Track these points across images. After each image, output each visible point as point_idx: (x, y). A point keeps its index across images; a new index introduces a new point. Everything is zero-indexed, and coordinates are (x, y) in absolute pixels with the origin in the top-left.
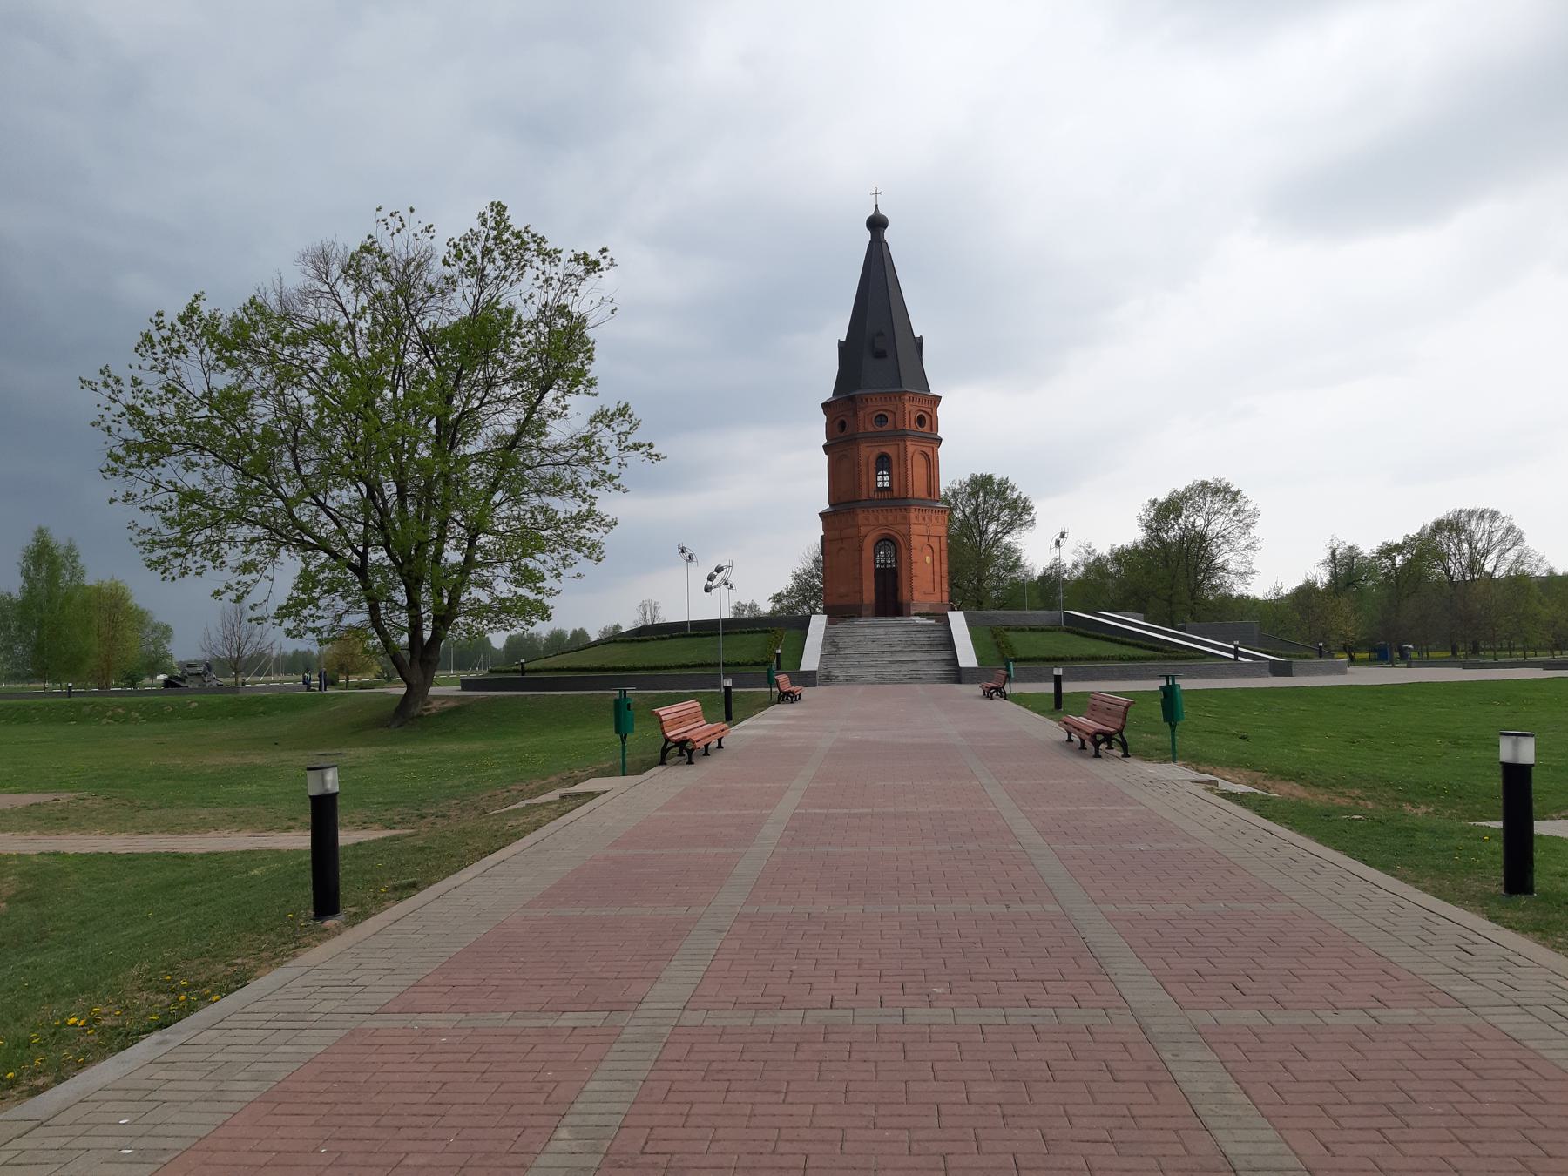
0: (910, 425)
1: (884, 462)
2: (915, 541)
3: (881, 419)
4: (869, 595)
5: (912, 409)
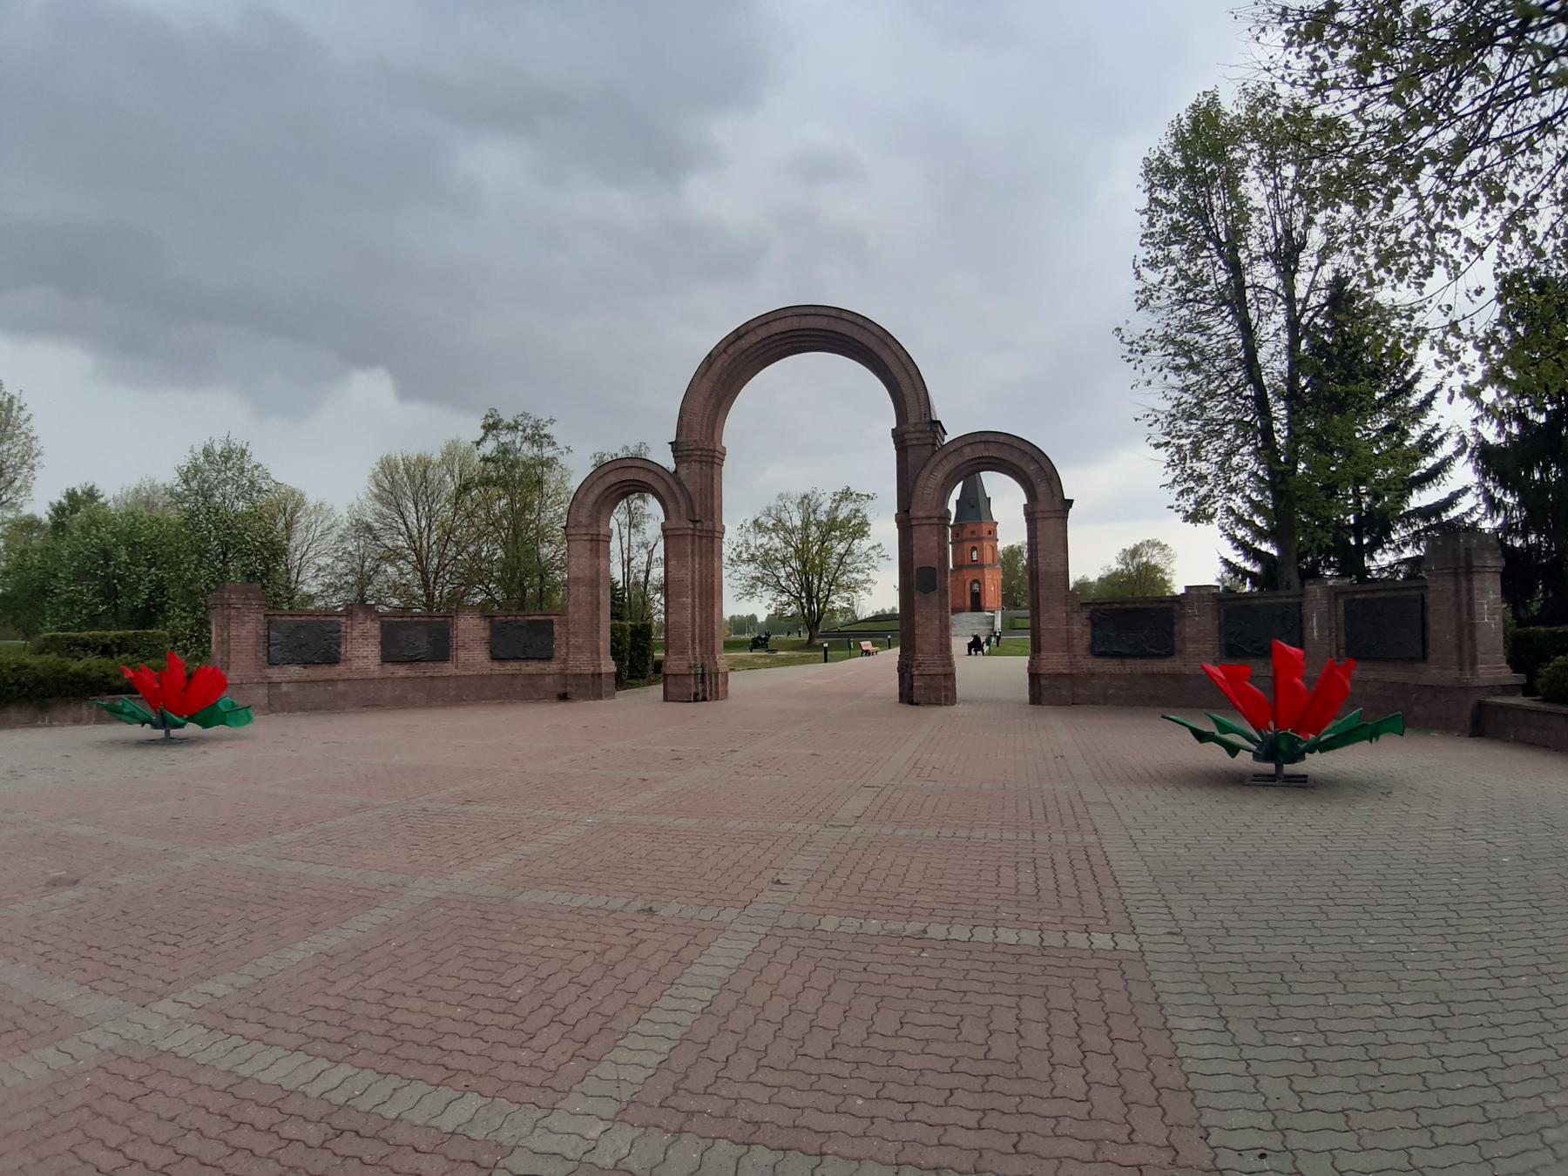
0: (985, 534)
1: (974, 548)
2: (987, 582)
3: (973, 532)
4: (968, 603)
5: (985, 528)
